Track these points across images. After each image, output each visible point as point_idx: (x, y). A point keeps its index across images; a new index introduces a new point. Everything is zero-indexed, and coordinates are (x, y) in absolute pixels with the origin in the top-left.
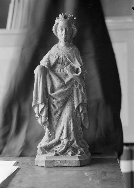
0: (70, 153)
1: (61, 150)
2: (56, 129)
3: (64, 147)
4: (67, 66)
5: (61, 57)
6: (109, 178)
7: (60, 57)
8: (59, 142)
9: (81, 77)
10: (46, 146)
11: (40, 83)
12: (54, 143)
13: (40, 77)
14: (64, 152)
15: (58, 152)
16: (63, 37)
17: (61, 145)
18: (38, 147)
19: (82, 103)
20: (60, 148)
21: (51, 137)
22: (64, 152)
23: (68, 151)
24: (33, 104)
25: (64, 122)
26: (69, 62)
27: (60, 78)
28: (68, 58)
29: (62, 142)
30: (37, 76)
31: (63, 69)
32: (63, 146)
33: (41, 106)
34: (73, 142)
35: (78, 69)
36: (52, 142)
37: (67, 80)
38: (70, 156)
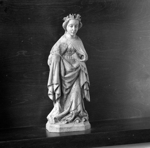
0: (77, 121)
1: (71, 120)
2: (65, 104)
3: (73, 116)
4: (74, 53)
5: (69, 47)
6: (57, 127)
7: (68, 47)
8: (68, 113)
9: (86, 62)
10: (59, 117)
11: (55, 68)
12: (65, 114)
13: (56, 63)
14: (73, 120)
15: (69, 121)
16: (73, 32)
17: (70, 115)
18: (49, 117)
19: (86, 82)
20: (69, 118)
21: (61, 110)
22: (73, 120)
23: (76, 119)
24: (49, 84)
25: (73, 97)
26: (75, 51)
27: (69, 63)
28: (74, 47)
29: (71, 112)
30: (54, 63)
31: (71, 56)
32: (71, 116)
33: (55, 87)
34: (80, 112)
35: (82, 56)
36: (64, 113)
37: (75, 66)
38: (78, 123)
